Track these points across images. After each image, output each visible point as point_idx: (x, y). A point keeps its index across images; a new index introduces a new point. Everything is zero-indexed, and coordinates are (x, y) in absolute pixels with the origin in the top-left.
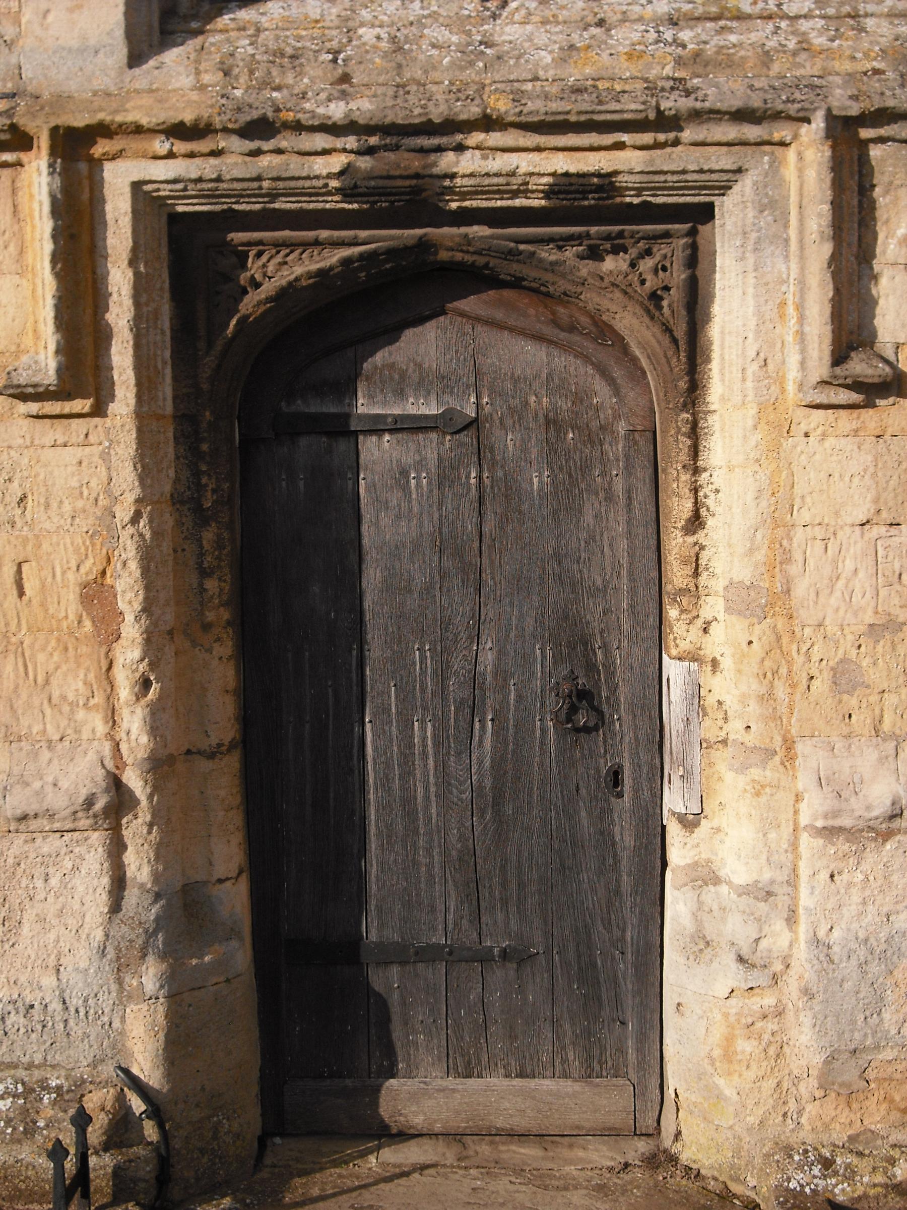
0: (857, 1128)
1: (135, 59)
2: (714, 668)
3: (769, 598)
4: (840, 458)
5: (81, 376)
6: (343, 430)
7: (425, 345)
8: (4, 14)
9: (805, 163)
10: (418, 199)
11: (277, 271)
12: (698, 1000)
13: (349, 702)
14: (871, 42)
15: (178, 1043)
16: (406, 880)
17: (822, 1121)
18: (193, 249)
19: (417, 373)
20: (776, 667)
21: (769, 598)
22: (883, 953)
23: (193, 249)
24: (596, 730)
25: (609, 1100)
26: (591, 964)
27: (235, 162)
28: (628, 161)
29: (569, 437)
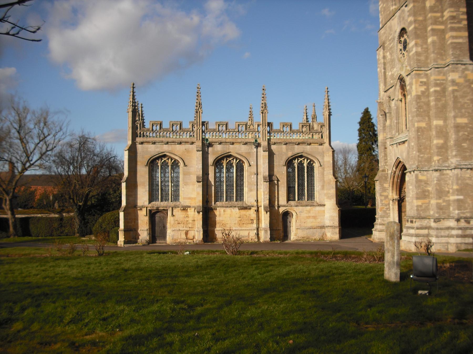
0: (176, 305)
1: (287, 202)
2: (168, 225)
3: (170, 223)
4: (172, 218)
5: (147, 215)
6: (155, 217)
7: (158, 214)
8: (471, 218)
9: (171, 208)
10: (158, 209)
11: (153, 212)
12: (168, 237)
13: (155, 227)
14: (12, 156)
15: (149, 238)
16: (157, 234)
17: (172, 241)
18: (150, 211)
19: (158, 215)
20: (170, 225)
21: (170, 223)
22: (174, 235)
23: (150, 211)
24: (164, 228)
25: (164, 242)
26: (164, 236)
27: (152, 208)
28: (165, 208)
29: (164, 217)
